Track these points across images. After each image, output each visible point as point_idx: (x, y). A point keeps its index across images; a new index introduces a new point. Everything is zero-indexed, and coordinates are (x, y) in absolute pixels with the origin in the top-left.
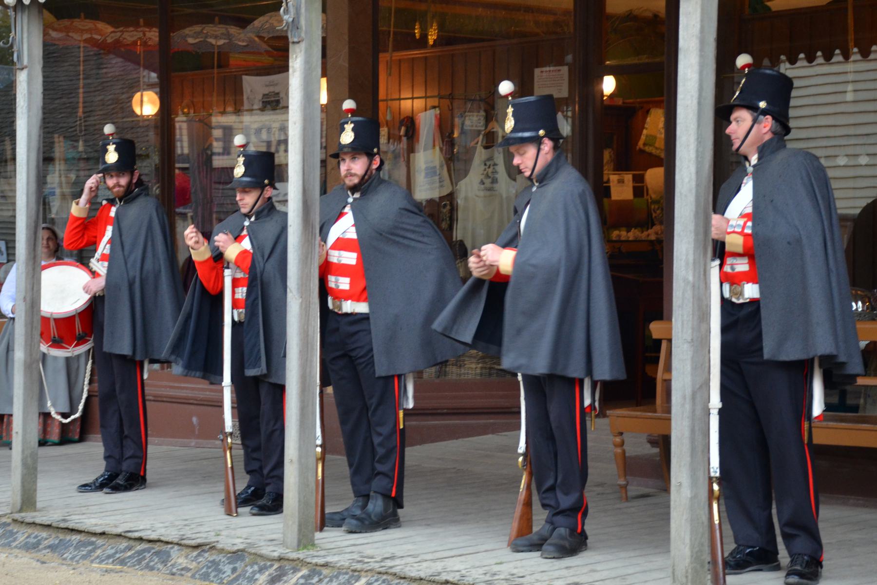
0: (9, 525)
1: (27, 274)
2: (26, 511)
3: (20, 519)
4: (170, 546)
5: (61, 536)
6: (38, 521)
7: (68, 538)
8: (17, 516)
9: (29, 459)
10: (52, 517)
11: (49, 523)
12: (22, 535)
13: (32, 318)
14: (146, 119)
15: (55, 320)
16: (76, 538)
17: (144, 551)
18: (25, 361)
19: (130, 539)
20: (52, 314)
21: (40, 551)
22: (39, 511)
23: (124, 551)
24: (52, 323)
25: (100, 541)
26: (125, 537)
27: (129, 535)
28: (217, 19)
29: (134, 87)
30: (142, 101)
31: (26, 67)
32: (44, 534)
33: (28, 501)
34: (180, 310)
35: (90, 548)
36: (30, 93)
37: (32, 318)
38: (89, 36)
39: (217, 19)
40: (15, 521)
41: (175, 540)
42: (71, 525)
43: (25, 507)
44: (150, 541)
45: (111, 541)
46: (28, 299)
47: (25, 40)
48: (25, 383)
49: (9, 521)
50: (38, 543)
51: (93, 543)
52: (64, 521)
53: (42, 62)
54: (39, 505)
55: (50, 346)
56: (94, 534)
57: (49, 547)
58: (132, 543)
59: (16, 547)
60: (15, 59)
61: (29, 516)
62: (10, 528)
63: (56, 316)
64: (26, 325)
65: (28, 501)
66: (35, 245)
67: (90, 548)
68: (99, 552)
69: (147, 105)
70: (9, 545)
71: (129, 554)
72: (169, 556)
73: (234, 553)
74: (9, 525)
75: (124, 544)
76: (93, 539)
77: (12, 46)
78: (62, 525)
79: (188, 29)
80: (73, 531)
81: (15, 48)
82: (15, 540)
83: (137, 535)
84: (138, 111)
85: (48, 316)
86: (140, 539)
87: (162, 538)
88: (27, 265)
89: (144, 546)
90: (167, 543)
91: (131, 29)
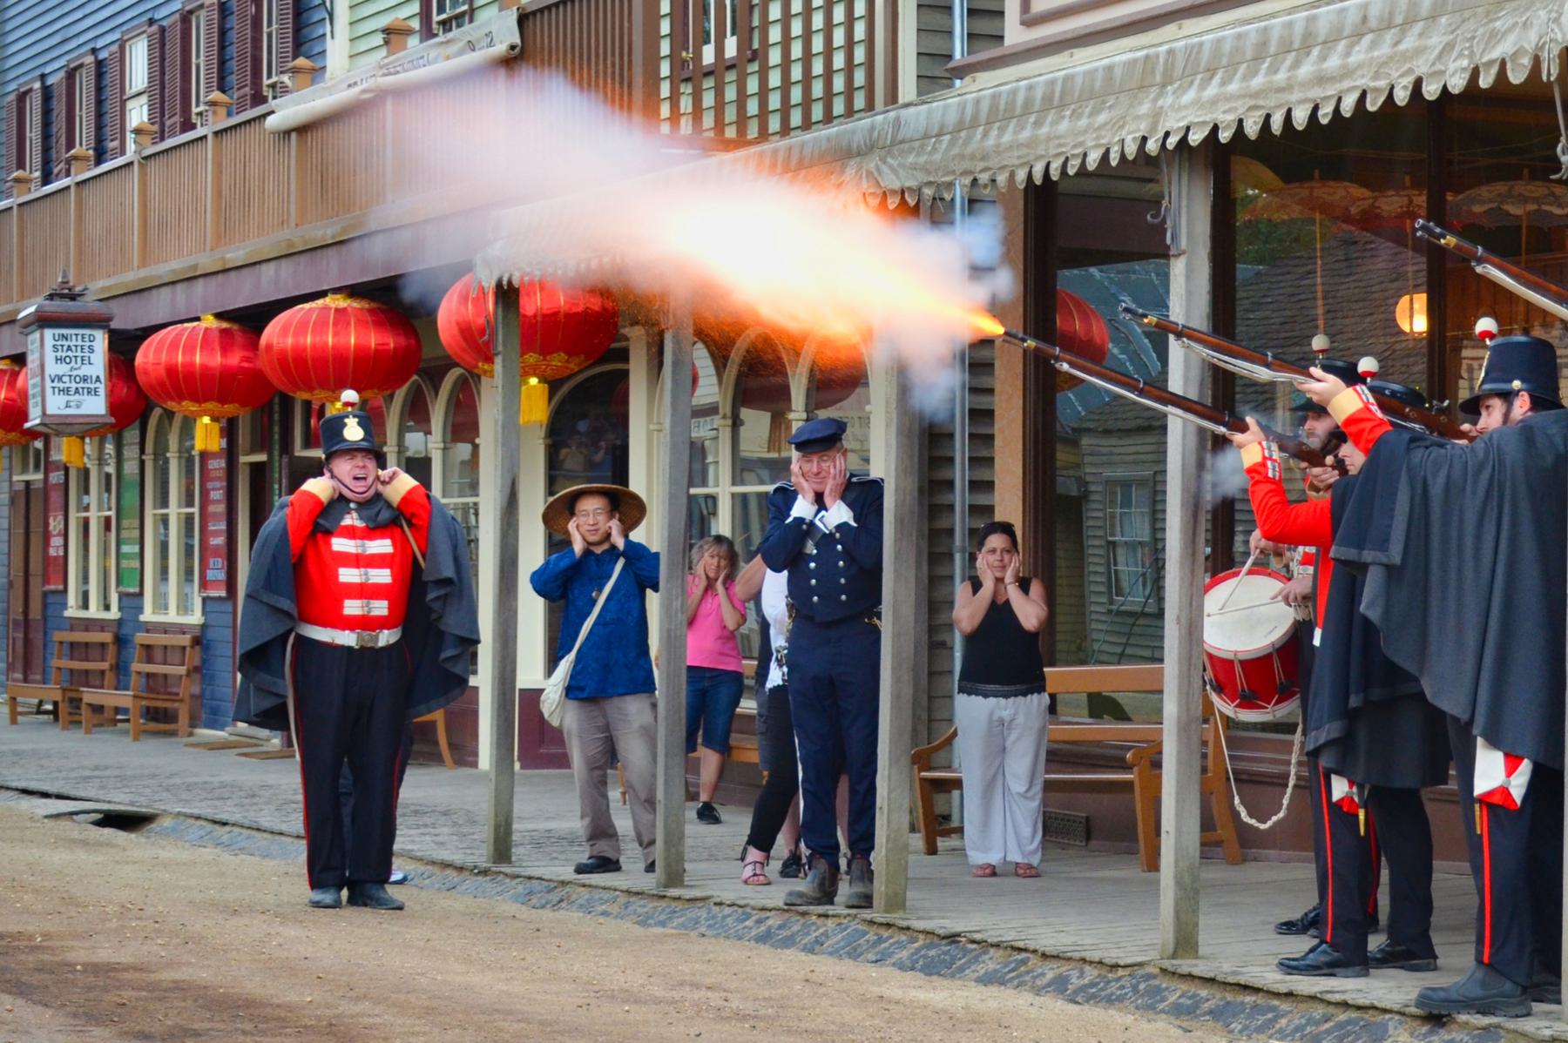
0: (1155, 977)
1: (1182, 579)
2: (1182, 958)
3: (1171, 969)
4: (1388, 1016)
5: (1229, 997)
6: (1196, 972)
7: (1240, 998)
8: (1167, 964)
9: (1186, 875)
10: (1223, 967)
11: (1211, 975)
12: (1176, 992)
13: (1191, 650)
14: (1416, 339)
15: (1243, 663)
16: (1249, 999)
17: (1349, 1022)
18: (1179, 718)
19: (1329, 1003)
20: (1236, 653)
21: (1197, 1017)
22: (1202, 958)
23: (1317, 1023)
24: (1238, 668)
25: (1285, 1006)
26: (1322, 1000)
27: (1329, 997)
28: (1526, 171)
29: (1400, 286)
30: (1412, 308)
31: (1184, 253)
32: (1204, 993)
33: (1186, 942)
34: (661, 364)
35: (1270, 1016)
36: (1189, 293)
37: (1191, 650)
38: (1535, 207)
39: (1526, 171)
40: (1163, 971)
41: (1396, 1007)
42: (1243, 980)
43: (1180, 952)
44: (1359, 1008)
45: (1303, 1006)
46: (1183, 621)
47: (1184, 211)
48: (1179, 753)
49: (1156, 971)
50: (1196, 1006)
51: (1274, 1009)
52: (1234, 973)
53: (1208, 244)
54: (1202, 951)
55: (1238, 706)
56: (1277, 995)
57: (1211, 1012)
58: (1331, 1010)
59: (1162, 1011)
60: (1168, 241)
61: (1185, 965)
62: (1156, 982)
63: (1242, 657)
64: (1180, 662)
65: (1186, 942)
66: (1194, 534)
67: (1270, 1016)
68: (1283, 1022)
69: (1415, 318)
70: (1151, 1007)
71: (1327, 1026)
72: (1386, 1031)
73: (1483, 1029)
74: (1155, 977)
75: (1319, 1011)
76: (1276, 1002)
77: (1164, 221)
78: (1231, 979)
79: (1484, 188)
80: (1246, 988)
81: (1169, 224)
82: (1163, 1000)
83: (1338, 997)
84: (1406, 328)
85: (1230, 656)
86: (1345, 1005)
87: (1377, 1004)
88: (1182, 564)
89: (1354, 1014)
90: (1385, 1011)
91: (1391, 193)
